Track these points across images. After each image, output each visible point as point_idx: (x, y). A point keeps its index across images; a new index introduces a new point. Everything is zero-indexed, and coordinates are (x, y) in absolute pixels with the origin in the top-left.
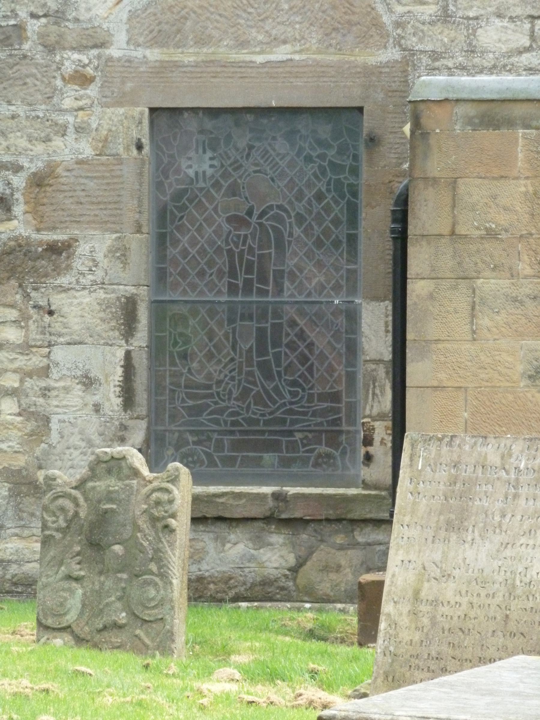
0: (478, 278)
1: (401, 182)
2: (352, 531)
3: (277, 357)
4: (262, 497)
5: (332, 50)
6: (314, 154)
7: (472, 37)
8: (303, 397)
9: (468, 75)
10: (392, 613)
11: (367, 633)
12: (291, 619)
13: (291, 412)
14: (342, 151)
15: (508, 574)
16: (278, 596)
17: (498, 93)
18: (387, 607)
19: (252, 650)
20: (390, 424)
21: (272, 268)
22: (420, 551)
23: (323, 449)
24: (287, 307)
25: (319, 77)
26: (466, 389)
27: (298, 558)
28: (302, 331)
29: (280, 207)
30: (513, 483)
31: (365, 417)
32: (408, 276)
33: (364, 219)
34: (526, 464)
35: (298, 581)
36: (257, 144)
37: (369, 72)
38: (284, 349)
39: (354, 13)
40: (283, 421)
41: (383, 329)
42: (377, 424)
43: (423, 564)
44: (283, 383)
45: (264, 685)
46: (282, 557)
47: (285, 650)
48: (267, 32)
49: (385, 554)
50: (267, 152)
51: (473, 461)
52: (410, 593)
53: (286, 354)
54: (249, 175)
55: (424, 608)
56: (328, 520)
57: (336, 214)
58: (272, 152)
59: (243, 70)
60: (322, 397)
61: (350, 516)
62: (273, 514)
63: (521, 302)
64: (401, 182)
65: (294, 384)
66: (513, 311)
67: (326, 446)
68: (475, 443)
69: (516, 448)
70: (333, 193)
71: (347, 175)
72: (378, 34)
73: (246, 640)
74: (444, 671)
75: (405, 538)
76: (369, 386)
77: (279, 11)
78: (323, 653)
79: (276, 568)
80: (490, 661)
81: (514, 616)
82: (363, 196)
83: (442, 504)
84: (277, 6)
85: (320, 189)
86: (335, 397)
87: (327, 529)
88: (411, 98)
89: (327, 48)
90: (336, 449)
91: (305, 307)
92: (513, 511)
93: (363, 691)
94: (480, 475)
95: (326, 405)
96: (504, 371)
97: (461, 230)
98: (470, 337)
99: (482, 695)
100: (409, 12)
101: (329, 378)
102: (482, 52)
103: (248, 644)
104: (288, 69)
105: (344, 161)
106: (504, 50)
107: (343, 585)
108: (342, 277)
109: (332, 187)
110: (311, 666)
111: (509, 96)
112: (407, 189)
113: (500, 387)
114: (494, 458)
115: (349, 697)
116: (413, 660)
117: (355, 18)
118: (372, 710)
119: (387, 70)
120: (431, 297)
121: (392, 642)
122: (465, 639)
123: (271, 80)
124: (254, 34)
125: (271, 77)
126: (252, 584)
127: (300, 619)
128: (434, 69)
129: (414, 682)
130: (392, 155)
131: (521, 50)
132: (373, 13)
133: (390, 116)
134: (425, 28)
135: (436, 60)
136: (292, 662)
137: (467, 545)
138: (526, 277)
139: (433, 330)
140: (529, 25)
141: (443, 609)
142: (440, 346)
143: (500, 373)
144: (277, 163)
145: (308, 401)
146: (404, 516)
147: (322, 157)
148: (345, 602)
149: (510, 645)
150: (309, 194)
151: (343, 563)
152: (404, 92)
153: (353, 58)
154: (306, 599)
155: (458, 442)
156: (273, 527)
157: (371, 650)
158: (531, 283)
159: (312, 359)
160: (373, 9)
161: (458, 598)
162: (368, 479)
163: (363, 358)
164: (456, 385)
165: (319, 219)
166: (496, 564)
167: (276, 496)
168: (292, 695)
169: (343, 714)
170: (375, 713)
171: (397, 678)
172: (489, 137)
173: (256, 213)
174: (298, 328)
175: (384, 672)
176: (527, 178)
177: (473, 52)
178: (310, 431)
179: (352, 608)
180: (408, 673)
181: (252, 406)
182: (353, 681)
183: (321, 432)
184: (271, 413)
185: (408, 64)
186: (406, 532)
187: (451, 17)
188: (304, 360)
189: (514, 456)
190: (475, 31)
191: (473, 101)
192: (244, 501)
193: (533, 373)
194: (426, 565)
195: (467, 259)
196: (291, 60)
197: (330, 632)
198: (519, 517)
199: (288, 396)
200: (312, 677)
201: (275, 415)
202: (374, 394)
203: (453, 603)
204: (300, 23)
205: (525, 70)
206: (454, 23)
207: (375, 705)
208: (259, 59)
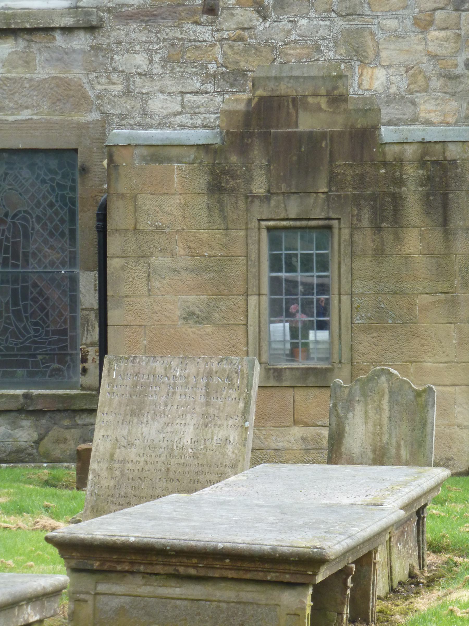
0: (152, 257)
1: (102, 196)
2: (74, 417)
3: (25, 307)
4: (17, 396)
5: (57, 113)
6: (47, 178)
7: (145, 105)
8: (42, 333)
9: (143, 129)
10: (97, 469)
11: (81, 482)
12: (34, 474)
13: (34, 342)
14: (65, 176)
15: (169, 442)
16: (27, 459)
17: (161, 140)
18: (93, 465)
19: (8, 494)
20: (97, 348)
21: (21, 250)
22: (114, 430)
23: (55, 365)
24: (31, 275)
25: (49, 130)
26: (145, 326)
27: (39, 435)
28: (41, 290)
29: (25, 212)
30: (172, 385)
31: (82, 345)
32: (108, 255)
33: (80, 220)
34: (180, 373)
35: (40, 449)
36: (10, 172)
37: (82, 128)
38: (29, 302)
40: (29, 348)
41: (93, 288)
42: (90, 349)
43: (116, 438)
44: (30, 324)
45: (15, 516)
46: (29, 434)
47: (29, 493)
48: (15, 101)
49: (93, 430)
50: (17, 177)
51: (148, 372)
52: (108, 456)
53: (31, 305)
54: (5, 191)
55: (116, 465)
56: (59, 411)
57: (62, 216)
58: (20, 176)
60: (55, 333)
61: (73, 407)
62: (23, 407)
63: (178, 272)
64: (102, 196)
65: (36, 324)
66: (174, 277)
67: (58, 363)
68: (149, 361)
69: (174, 363)
70: (60, 203)
72: (86, 103)
73: (5, 488)
74: (129, 504)
75: (105, 422)
76: (85, 325)
77: (23, 88)
78: (54, 495)
79: (26, 442)
80: (158, 497)
81: (172, 468)
82: (78, 204)
83: (128, 400)
84: (21, 85)
85: (51, 201)
86: (64, 332)
87: (58, 416)
88: (107, 144)
89: (54, 111)
90: (64, 366)
91: (43, 275)
92: (172, 403)
93: (78, 518)
94: (152, 380)
95: (57, 337)
96: (168, 315)
97: (140, 227)
98: (147, 294)
99: (150, 520)
100: (105, 89)
101: (59, 320)
102: (151, 115)
103: (6, 490)
104: (29, 125)
105: (66, 183)
106: (165, 114)
108: (66, 256)
109: (59, 199)
110: (46, 503)
111: (168, 143)
112: (105, 201)
113: (166, 325)
114: (160, 370)
115: (69, 522)
116: (109, 498)
117: (71, 93)
118: (80, 532)
119: (92, 126)
120: (123, 268)
121: (96, 487)
122: (142, 483)
124: (7, 103)
125: (18, 130)
126: (10, 452)
127: (39, 474)
128: (122, 125)
129: (110, 512)
130: (97, 179)
131: (176, 113)
132: (82, 89)
133: (95, 154)
134: (116, 99)
136: (33, 501)
137: (143, 425)
138: (181, 256)
139: (124, 289)
140: (181, 98)
141: (128, 465)
142: (129, 299)
143: (166, 316)
144: (23, 184)
145: (46, 335)
146: (104, 407)
147: (52, 180)
148: (69, 462)
149: (170, 487)
150: (44, 204)
151: (68, 437)
152: (103, 139)
154: (45, 460)
155: (138, 360)
156: (24, 415)
157: (84, 492)
158: (184, 259)
159: (48, 308)
160: (82, 87)
161: (138, 459)
162: (84, 384)
163: (81, 307)
164: (139, 324)
165: (51, 220)
166: (162, 436)
167: (26, 396)
168: (33, 522)
169: (61, 534)
170: (82, 534)
171: (99, 509)
172: (156, 168)
173: (11, 215)
174: (38, 289)
175: (91, 506)
176: (180, 194)
177: (146, 114)
179: (73, 466)
180: (106, 507)
181: (9, 339)
182: (73, 512)
183: (54, 354)
184: (21, 343)
185: (105, 122)
186: (106, 418)
187: (132, 92)
188: (42, 308)
189: (173, 368)
190: (147, 101)
191: (146, 145)
192: (4, 399)
193: (186, 316)
194: (118, 438)
195: (144, 245)
196: (31, 119)
197: (59, 481)
198: (176, 407)
199: (33, 333)
200: (46, 511)
201: (25, 344)
202: (88, 330)
203: (134, 461)
204: (37, 96)
205: (178, 126)
206: (134, 96)
207: (81, 528)
208: (11, 118)
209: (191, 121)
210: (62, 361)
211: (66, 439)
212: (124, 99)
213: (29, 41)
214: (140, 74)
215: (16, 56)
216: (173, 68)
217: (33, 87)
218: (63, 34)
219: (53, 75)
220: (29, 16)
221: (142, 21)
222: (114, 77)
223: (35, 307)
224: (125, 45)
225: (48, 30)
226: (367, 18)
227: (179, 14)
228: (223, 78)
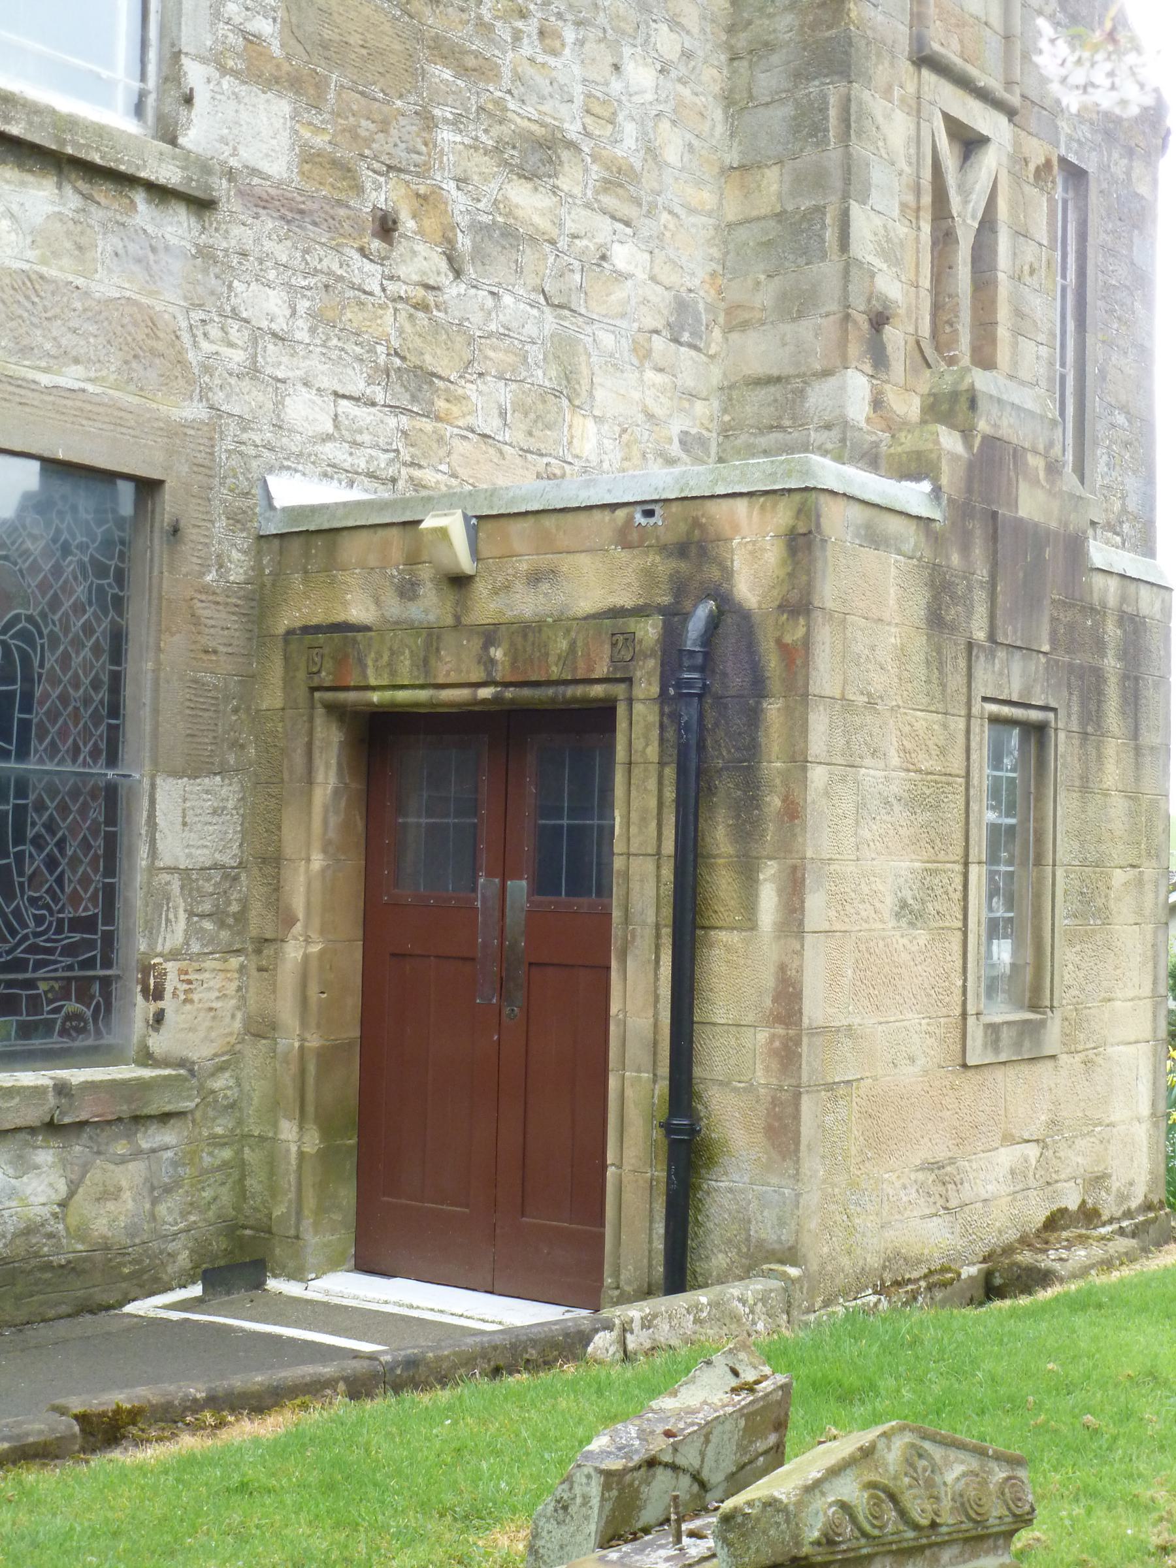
23: (72, 1006)
29: (30, 619)
35: (69, 1220)
37: (175, 431)
38: (28, 848)
39: (158, 338)
46: (51, 1185)
48: (55, 339)
59: (22, 392)
71: (111, 580)
107: (122, 1218)
123: (58, 416)
130: (195, 560)
135: (244, 430)
145: (59, 930)
151: (124, 1183)
153: (155, 406)
160: (177, 337)
178: (56, 979)
183: (69, 979)
190: (283, 398)
192: (17, 1100)
196: (84, 391)
199: (32, 924)
202: (168, 920)
208: (45, 379)
209: (350, 459)
210: (84, 996)
211: (120, 1189)
212: (246, 384)
213: (87, 197)
214: (274, 335)
215: (59, 225)
216: (328, 339)
217: (90, 314)
218: (149, 201)
219: (128, 294)
220: (101, 136)
221: (283, 218)
222: (234, 326)
223: (39, 861)
224: (251, 263)
225: (123, 180)
226: (581, 319)
227: (340, 222)
228: (400, 378)
